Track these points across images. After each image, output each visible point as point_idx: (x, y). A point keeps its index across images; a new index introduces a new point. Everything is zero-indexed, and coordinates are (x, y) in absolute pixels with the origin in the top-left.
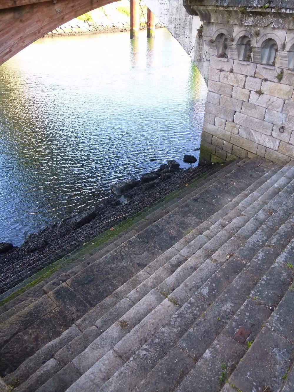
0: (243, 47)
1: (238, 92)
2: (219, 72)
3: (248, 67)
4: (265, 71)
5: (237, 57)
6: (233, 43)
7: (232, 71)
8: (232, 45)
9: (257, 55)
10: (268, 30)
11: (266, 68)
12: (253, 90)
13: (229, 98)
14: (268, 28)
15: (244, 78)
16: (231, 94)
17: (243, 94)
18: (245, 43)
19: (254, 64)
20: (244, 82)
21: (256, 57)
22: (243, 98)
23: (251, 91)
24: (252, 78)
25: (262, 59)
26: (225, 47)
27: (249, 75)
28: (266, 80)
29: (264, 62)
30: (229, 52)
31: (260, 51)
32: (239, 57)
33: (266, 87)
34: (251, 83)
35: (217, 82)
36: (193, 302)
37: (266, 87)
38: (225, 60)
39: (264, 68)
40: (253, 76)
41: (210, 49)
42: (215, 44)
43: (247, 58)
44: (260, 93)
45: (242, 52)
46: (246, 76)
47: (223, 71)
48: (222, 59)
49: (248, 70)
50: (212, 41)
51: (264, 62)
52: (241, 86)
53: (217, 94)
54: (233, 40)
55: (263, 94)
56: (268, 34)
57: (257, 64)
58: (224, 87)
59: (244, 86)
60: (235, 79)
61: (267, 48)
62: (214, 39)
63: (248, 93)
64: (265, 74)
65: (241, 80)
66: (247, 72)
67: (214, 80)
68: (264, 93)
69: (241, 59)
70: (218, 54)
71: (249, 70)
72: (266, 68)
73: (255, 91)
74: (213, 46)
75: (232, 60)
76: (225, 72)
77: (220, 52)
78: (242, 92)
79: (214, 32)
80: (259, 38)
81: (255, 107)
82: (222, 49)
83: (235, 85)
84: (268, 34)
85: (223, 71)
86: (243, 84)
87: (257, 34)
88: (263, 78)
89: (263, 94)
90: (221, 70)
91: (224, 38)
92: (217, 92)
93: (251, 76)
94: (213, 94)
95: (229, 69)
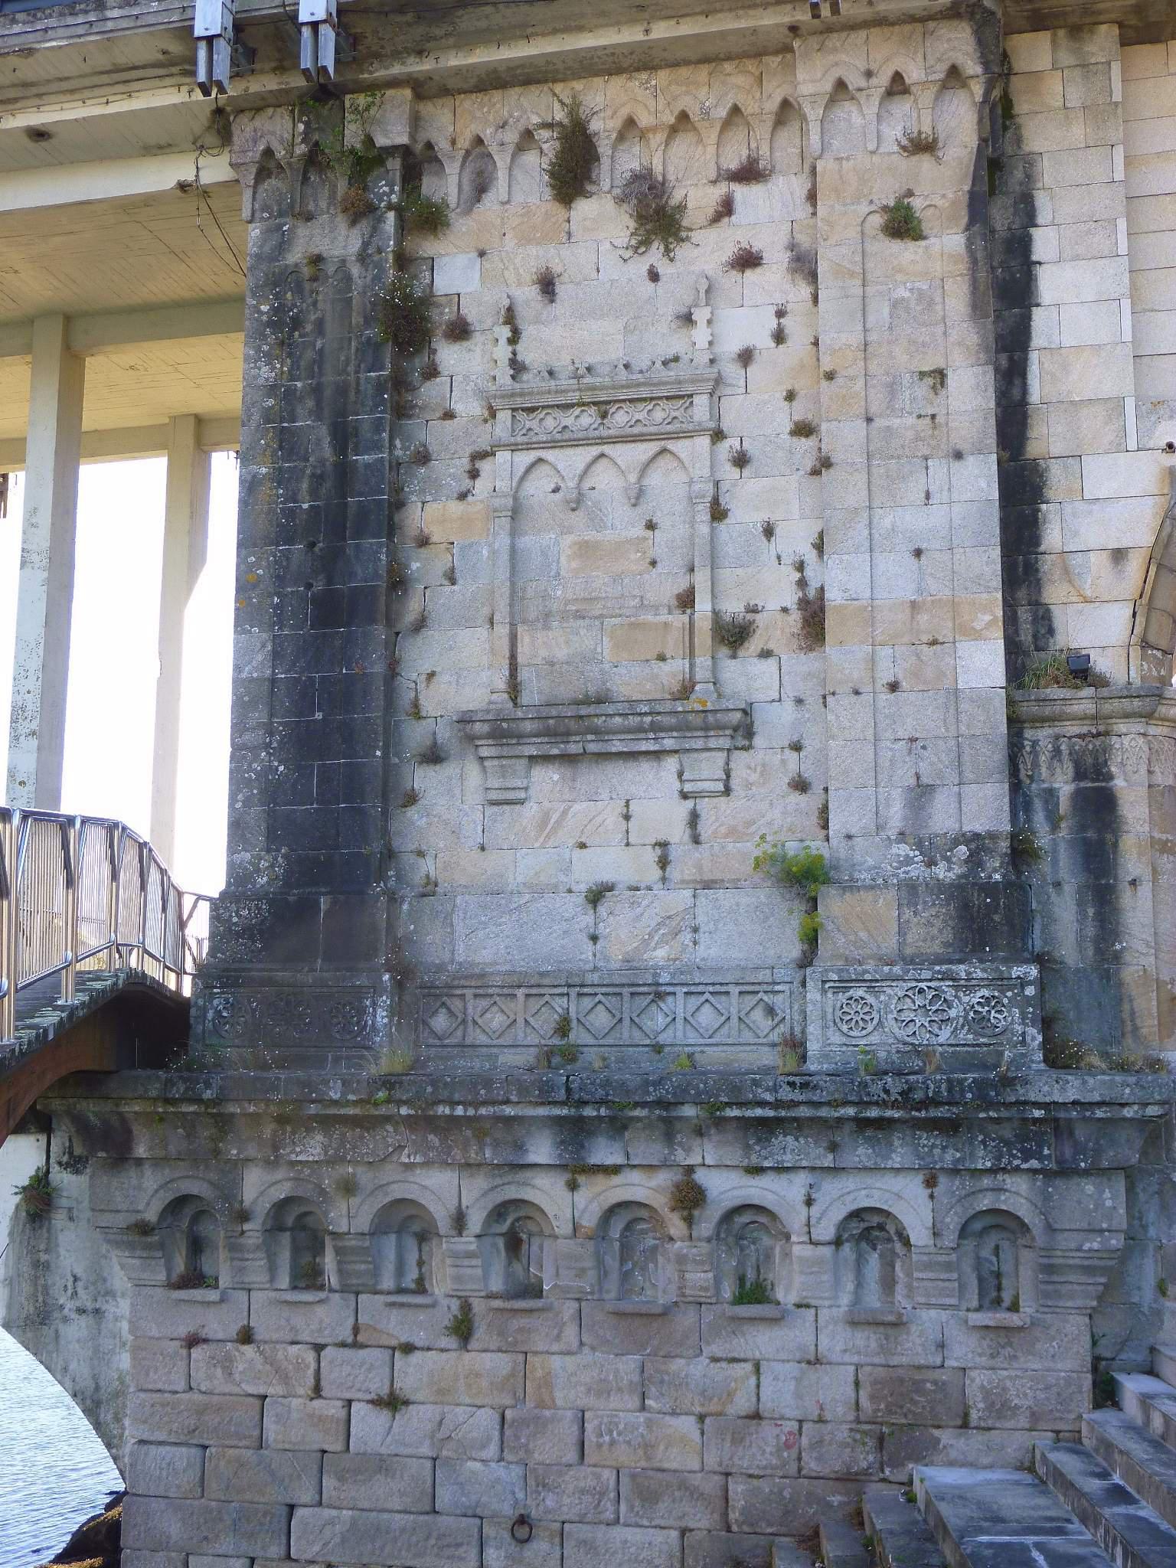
0: (286, 1238)
1: (295, 1415)
2: (184, 1352)
3: (320, 1311)
4: (395, 1315)
5: (267, 1278)
6: (246, 1227)
7: (246, 1336)
8: (243, 1232)
9: (355, 1262)
10: (389, 1173)
11: (402, 1305)
12: (360, 1395)
13: (250, 1452)
14: (388, 1167)
15: (310, 1356)
16: (257, 1433)
17: (318, 1420)
18: (290, 1221)
19: (346, 1295)
20: (311, 1372)
21: (349, 1267)
22: (317, 1439)
23: (349, 1402)
24: (347, 1353)
25: (376, 1273)
26: (197, 1246)
27: (328, 1340)
28: (408, 1348)
29: (388, 1282)
30: (220, 1264)
31: (367, 1244)
32: (272, 1280)
33: (412, 1374)
34: (347, 1369)
35: (176, 1392)
36: (546, 1132)
37: (412, 1374)
38: (213, 1295)
39: (393, 1304)
40: (350, 1340)
41: (130, 1261)
42: (155, 1238)
43: (308, 1277)
44: (393, 1402)
45: (285, 1257)
46: (319, 1348)
47: (206, 1341)
48: (197, 1294)
49: (321, 1322)
50: (143, 1229)
51: (388, 1282)
52: (301, 1391)
53: (184, 1449)
54: (244, 1216)
55: (407, 1403)
56: (388, 1184)
57: (357, 1294)
58: (219, 1409)
59: (317, 1391)
60: (268, 1367)
61: (386, 1233)
62: (151, 1215)
63: (343, 1413)
64: (397, 1326)
65: (300, 1366)
66: (320, 1330)
67: (159, 1386)
68: (412, 1398)
69: (284, 1281)
70: (169, 1276)
71: (327, 1320)
72: (402, 1305)
73: (371, 1402)
74: (149, 1247)
75: (242, 1296)
76: (213, 1346)
77: (180, 1265)
78: (311, 1416)
79: (150, 1192)
80: (354, 1201)
81: (381, 1465)
82: (184, 1253)
83: (271, 1391)
84: (388, 1184)
85: (206, 1341)
86: (311, 1382)
87: (349, 1188)
88: (394, 1343)
89: (407, 1403)
90: (193, 1341)
91: (189, 1211)
92: (183, 1438)
93: (343, 1345)
94: (163, 1450)
95: (233, 1331)
